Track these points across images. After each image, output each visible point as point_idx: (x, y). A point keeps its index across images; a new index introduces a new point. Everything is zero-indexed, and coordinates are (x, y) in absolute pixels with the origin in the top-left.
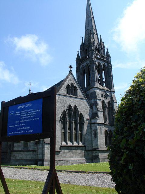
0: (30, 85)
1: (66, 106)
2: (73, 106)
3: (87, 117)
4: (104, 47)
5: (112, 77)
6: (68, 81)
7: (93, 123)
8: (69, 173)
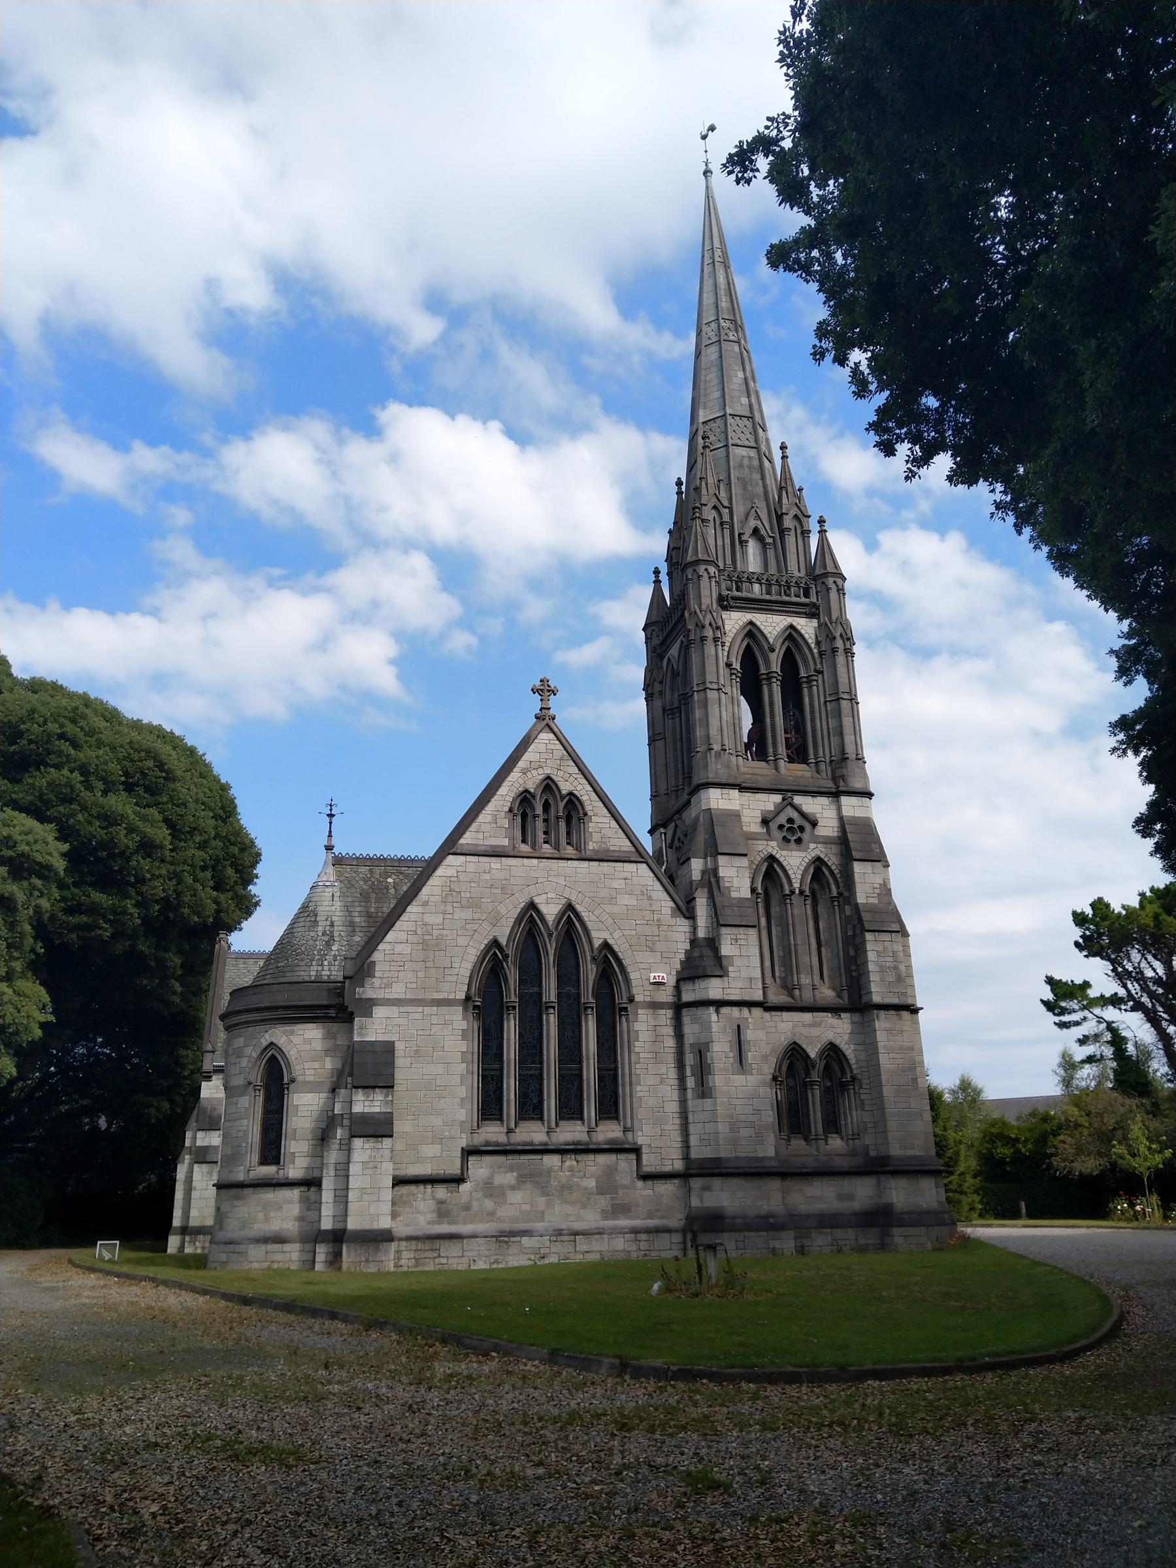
0: (331, 816)
1: (510, 911)
2: (551, 911)
3: (652, 971)
4: (801, 517)
5: (853, 700)
6: (524, 772)
7: (690, 1005)
8: (482, 859)
